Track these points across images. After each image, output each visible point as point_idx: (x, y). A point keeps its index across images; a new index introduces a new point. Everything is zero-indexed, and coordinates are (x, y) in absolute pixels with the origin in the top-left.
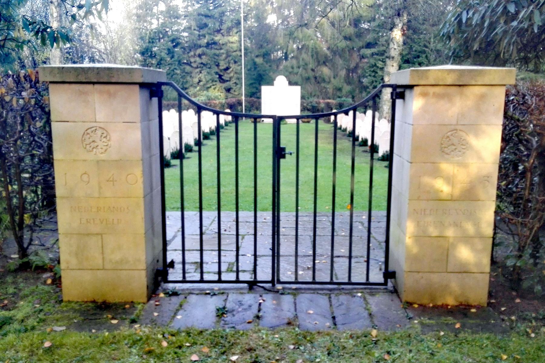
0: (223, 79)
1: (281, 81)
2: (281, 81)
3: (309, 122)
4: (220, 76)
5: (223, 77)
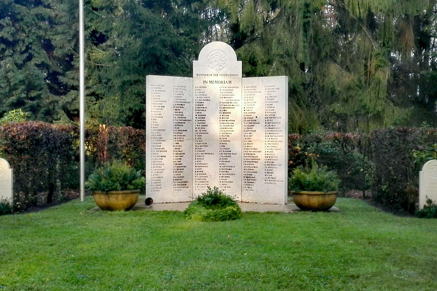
0: (59, 84)
1: (217, 58)
2: (217, 58)
3: (325, 208)
4: (53, 76)
5: (60, 78)
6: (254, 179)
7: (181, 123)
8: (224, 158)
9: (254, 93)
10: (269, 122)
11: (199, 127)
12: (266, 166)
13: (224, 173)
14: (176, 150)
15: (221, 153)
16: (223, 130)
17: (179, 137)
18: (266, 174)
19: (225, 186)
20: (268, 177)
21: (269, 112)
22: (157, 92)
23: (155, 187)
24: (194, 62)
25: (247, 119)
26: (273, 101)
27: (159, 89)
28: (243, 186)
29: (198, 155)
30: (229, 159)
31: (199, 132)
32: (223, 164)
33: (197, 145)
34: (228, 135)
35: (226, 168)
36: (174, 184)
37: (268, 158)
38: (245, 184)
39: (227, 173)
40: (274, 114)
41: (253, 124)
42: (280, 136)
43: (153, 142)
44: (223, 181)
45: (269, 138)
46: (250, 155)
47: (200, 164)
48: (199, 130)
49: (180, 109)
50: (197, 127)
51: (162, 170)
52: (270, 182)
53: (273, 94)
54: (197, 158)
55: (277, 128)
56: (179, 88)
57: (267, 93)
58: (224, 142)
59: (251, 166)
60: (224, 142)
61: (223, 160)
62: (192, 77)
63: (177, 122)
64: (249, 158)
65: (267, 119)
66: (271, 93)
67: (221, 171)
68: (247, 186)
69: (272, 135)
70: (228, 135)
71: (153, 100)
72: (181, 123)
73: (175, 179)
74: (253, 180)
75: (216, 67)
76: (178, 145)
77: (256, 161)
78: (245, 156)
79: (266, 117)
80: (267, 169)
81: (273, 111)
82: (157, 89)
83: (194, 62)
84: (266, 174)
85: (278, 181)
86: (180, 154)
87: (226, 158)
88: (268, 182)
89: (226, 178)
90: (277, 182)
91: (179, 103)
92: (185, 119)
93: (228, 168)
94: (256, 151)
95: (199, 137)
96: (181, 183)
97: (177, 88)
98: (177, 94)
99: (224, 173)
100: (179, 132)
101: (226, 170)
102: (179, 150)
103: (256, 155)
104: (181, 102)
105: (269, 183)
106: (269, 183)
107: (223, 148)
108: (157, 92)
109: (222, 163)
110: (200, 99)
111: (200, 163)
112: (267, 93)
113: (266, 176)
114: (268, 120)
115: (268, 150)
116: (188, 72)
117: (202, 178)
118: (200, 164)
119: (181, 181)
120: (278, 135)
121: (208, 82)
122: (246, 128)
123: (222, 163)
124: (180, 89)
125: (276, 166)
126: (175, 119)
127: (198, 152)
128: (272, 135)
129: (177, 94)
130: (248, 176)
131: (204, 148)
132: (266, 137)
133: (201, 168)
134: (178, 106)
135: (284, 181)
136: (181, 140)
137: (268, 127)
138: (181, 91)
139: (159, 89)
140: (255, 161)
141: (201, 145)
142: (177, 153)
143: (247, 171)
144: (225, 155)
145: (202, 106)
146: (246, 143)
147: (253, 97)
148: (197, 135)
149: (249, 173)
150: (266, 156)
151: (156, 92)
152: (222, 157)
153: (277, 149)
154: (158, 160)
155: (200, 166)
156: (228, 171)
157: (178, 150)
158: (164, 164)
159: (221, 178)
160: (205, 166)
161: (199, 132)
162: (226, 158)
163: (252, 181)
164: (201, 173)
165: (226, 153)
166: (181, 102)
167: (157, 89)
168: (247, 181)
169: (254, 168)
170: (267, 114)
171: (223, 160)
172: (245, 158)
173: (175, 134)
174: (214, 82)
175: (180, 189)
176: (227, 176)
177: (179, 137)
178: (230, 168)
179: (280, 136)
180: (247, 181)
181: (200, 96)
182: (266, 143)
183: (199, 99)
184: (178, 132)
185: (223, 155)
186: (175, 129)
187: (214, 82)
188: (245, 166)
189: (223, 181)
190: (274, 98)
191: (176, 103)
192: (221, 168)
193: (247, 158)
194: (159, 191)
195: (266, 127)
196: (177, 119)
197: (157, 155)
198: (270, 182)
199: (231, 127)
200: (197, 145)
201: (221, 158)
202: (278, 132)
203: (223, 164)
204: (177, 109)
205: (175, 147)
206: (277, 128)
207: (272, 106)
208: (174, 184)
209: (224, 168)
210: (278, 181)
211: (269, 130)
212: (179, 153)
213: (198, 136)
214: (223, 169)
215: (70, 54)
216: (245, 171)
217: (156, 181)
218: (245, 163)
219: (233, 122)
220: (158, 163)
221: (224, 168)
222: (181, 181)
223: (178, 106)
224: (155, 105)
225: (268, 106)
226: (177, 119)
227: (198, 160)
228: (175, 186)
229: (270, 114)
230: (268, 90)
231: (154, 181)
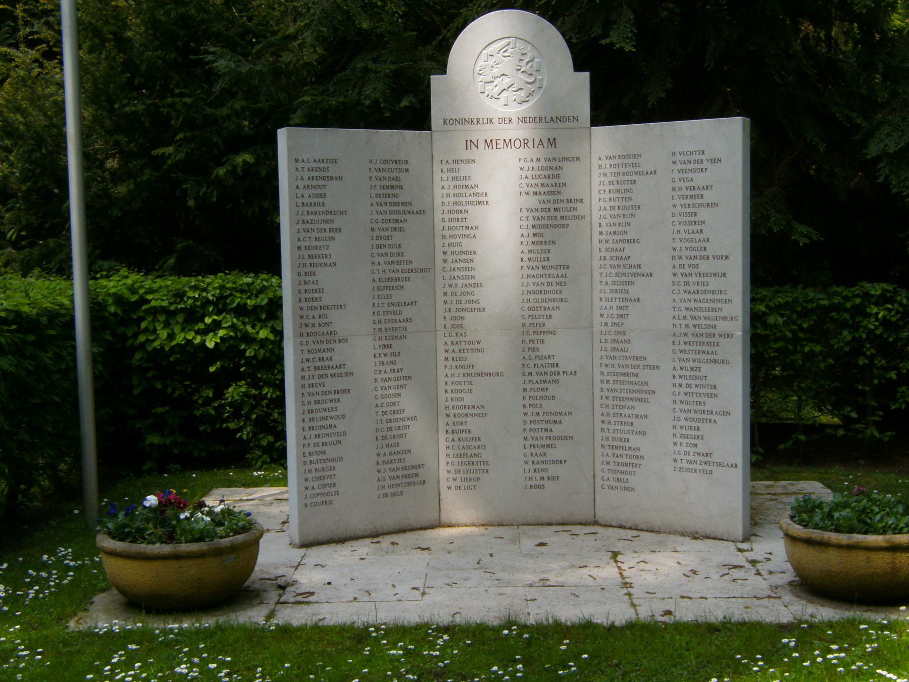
6: (636, 453)
7: (397, 279)
8: (536, 386)
9: (634, 177)
10: (687, 270)
11: (453, 289)
12: (678, 414)
13: (538, 435)
14: (383, 368)
15: (527, 370)
16: (532, 297)
17: (390, 325)
18: (678, 440)
19: (542, 474)
20: (684, 449)
21: (687, 240)
22: (314, 183)
23: (317, 491)
24: (435, 80)
25: (608, 262)
26: (700, 201)
27: (320, 174)
28: (599, 474)
29: (455, 379)
30: (552, 389)
31: (454, 307)
32: (535, 406)
33: (451, 348)
34: (548, 313)
35: (546, 418)
36: (381, 475)
37: (684, 389)
38: (606, 467)
39: (548, 434)
40: (704, 244)
41: (630, 279)
42: (725, 318)
43: (305, 348)
44: (536, 459)
45: (684, 322)
46: (622, 378)
47: (459, 407)
48: (454, 298)
49: (394, 233)
50: (447, 289)
51: (338, 434)
52: (690, 466)
53: (699, 179)
54: (449, 388)
55: (713, 292)
56: (386, 166)
57: (677, 176)
58: (535, 337)
59: (623, 412)
60: (535, 337)
61: (532, 394)
62: (429, 128)
63: (383, 276)
64: (619, 387)
65: (677, 263)
66: (690, 175)
67: (528, 427)
68: (611, 476)
69: (696, 314)
70: (548, 313)
71: (301, 209)
72: (397, 279)
73: (381, 459)
74: (631, 457)
75: (505, 94)
76: (388, 351)
77: (644, 396)
78: (605, 378)
79: (677, 254)
80: (679, 424)
81: (701, 236)
82: (314, 174)
83: (435, 80)
84: (678, 440)
85: (720, 464)
86: (398, 379)
87: (543, 386)
88: (685, 465)
89: (546, 450)
90: (715, 469)
91: (388, 217)
92: (410, 266)
93: (552, 418)
94: (641, 363)
95: (457, 322)
96: (400, 473)
97: (381, 166)
98: (383, 187)
99: (538, 435)
100: (392, 308)
101: (544, 426)
102: (392, 367)
103: (641, 379)
104: (396, 212)
105: (688, 470)
106: (688, 470)
107: (533, 354)
108: (314, 183)
109: (532, 402)
110: (457, 199)
111: (459, 403)
112: (677, 176)
113: (677, 448)
114: (682, 266)
115: (683, 364)
116: (575, 71)
117: (469, 452)
118: (459, 407)
119: (400, 465)
120: (718, 314)
121: (482, 144)
122: (607, 288)
123: (532, 402)
124: (392, 171)
125: (713, 417)
126: (376, 267)
127: (453, 371)
128: (696, 314)
129: (383, 187)
130: (615, 444)
131: (472, 358)
132: (677, 322)
133: (464, 419)
134: (384, 226)
135: (740, 465)
136: (398, 333)
137: (682, 288)
138: (394, 175)
139: (320, 174)
140: (638, 395)
141: (463, 346)
142: (386, 376)
143: (612, 427)
144: (539, 378)
145: (464, 224)
146: (609, 338)
147: (629, 191)
148: (448, 315)
149: (619, 435)
150: (678, 381)
151: (310, 183)
152: (531, 386)
153: (715, 361)
154: (325, 406)
155: (461, 415)
156: (549, 426)
157: (388, 368)
158: (344, 416)
159: (528, 451)
160: (478, 415)
161: (454, 307)
162: (543, 386)
163: (629, 461)
164: (464, 435)
165: (542, 370)
166: (396, 212)
167: (314, 174)
168: (611, 459)
169: (634, 420)
170: (678, 245)
171: (532, 394)
172: (605, 386)
173: (377, 318)
174: (501, 143)
175: (399, 489)
176: (548, 442)
177: (390, 325)
178: (558, 418)
179: (725, 318)
180: (611, 459)
181: (457, 191)
182: (677, 340)
183: (452, 199)
184: (386, 309)
185: (535, 378)
186: (376, 301)
187: (501, 143)
188: (605, 411)
189: (536, 459)
190: (705, 192)
191: (380, 217)
192: (528, 419)
193: (611, 386)
194: (331, 502)
195: (676, 288)
196: (383, 267)
197: (320, 389)
198: (690, 466)
199: (558, 288)
200: (451, 348)
201: (528, 386)
202: (719, 305)
203: (535, 406)
204: (383, 234)
205: (378, 360)
206: (713, 292)
207: (696, 219)
208: (381, 475)
209: (537, 418)
210: (720, 464)
211: (686, 296)
212: (392, 375)
213: (452, 318)
214: (537, 422)
215: (895, 191)
216: (605, 426)
217: (318, 474)
218: (605, 402)
219: (564, 272)
220: (324, 414)
221: (537, 418)
222: (400, 465)
223: (384, 226)
224: (309, 226)
225: (683, 219)
226: (383, 267)
227: (457, 420)
228: (381, 483)
229: (688, 245)
230: (680, 167)
231: (314, 474)
